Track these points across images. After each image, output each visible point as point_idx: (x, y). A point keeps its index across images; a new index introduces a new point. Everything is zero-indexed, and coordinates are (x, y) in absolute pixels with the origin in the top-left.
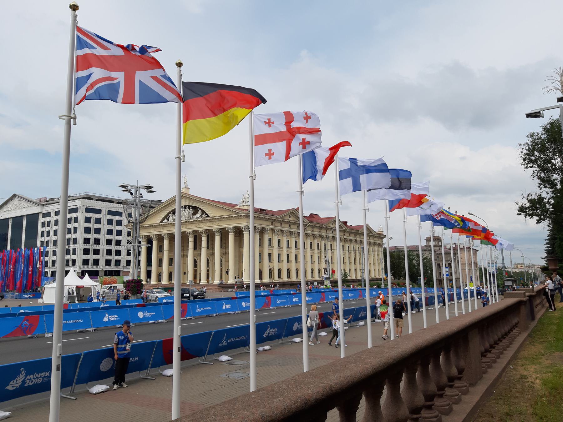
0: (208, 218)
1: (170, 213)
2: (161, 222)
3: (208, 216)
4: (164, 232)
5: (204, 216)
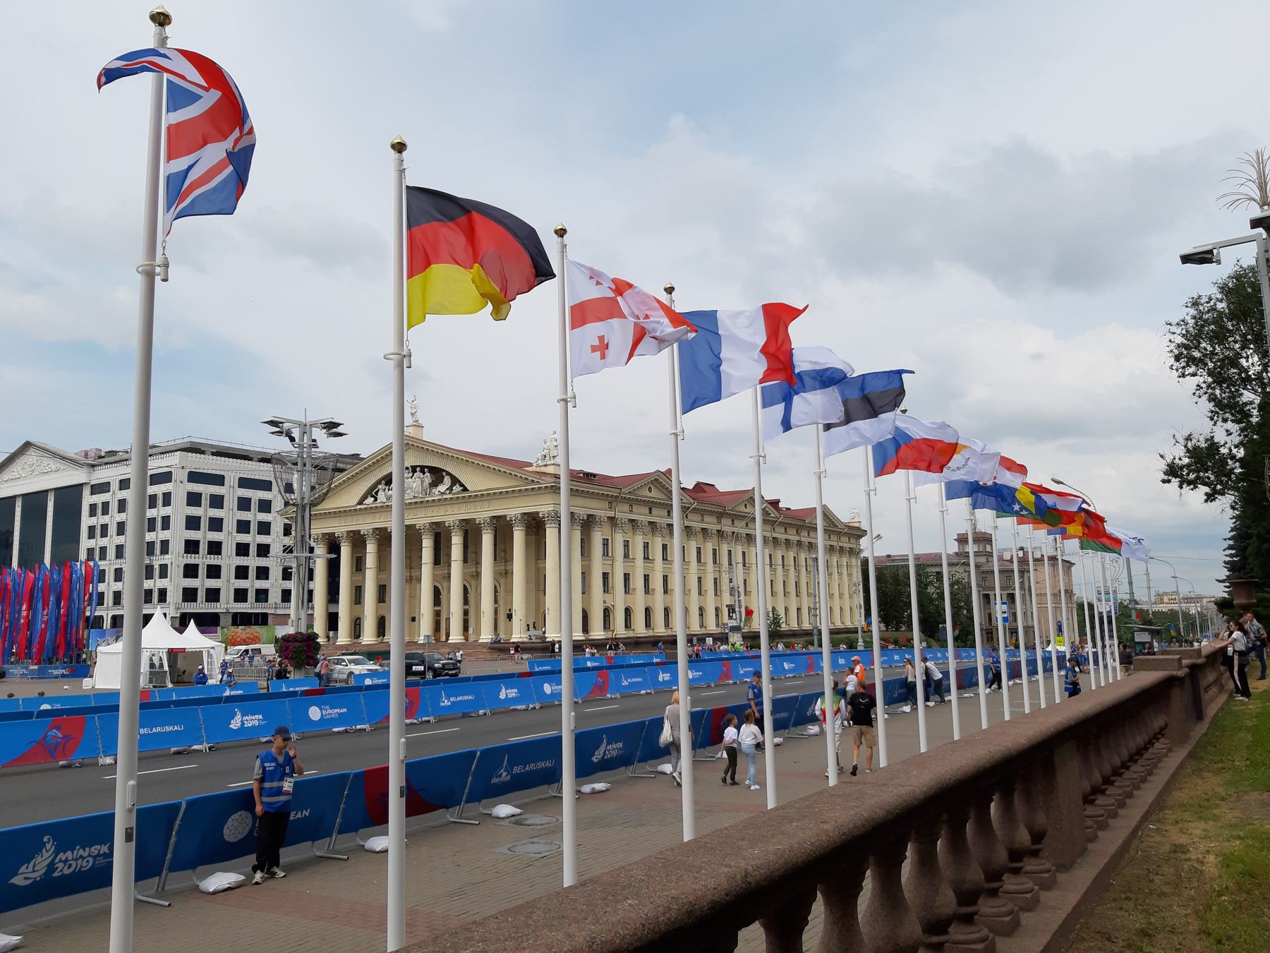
0: (466, 495)
1: (379, 482)
2: (360, 503)
3: (465, 489)
4: (365, 525)
5: (457, 488)
